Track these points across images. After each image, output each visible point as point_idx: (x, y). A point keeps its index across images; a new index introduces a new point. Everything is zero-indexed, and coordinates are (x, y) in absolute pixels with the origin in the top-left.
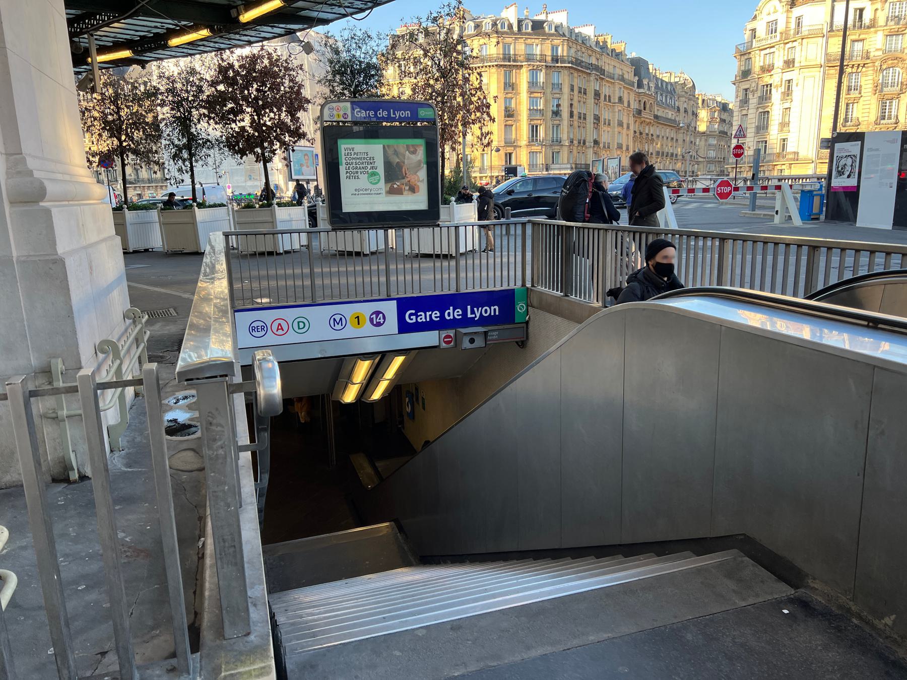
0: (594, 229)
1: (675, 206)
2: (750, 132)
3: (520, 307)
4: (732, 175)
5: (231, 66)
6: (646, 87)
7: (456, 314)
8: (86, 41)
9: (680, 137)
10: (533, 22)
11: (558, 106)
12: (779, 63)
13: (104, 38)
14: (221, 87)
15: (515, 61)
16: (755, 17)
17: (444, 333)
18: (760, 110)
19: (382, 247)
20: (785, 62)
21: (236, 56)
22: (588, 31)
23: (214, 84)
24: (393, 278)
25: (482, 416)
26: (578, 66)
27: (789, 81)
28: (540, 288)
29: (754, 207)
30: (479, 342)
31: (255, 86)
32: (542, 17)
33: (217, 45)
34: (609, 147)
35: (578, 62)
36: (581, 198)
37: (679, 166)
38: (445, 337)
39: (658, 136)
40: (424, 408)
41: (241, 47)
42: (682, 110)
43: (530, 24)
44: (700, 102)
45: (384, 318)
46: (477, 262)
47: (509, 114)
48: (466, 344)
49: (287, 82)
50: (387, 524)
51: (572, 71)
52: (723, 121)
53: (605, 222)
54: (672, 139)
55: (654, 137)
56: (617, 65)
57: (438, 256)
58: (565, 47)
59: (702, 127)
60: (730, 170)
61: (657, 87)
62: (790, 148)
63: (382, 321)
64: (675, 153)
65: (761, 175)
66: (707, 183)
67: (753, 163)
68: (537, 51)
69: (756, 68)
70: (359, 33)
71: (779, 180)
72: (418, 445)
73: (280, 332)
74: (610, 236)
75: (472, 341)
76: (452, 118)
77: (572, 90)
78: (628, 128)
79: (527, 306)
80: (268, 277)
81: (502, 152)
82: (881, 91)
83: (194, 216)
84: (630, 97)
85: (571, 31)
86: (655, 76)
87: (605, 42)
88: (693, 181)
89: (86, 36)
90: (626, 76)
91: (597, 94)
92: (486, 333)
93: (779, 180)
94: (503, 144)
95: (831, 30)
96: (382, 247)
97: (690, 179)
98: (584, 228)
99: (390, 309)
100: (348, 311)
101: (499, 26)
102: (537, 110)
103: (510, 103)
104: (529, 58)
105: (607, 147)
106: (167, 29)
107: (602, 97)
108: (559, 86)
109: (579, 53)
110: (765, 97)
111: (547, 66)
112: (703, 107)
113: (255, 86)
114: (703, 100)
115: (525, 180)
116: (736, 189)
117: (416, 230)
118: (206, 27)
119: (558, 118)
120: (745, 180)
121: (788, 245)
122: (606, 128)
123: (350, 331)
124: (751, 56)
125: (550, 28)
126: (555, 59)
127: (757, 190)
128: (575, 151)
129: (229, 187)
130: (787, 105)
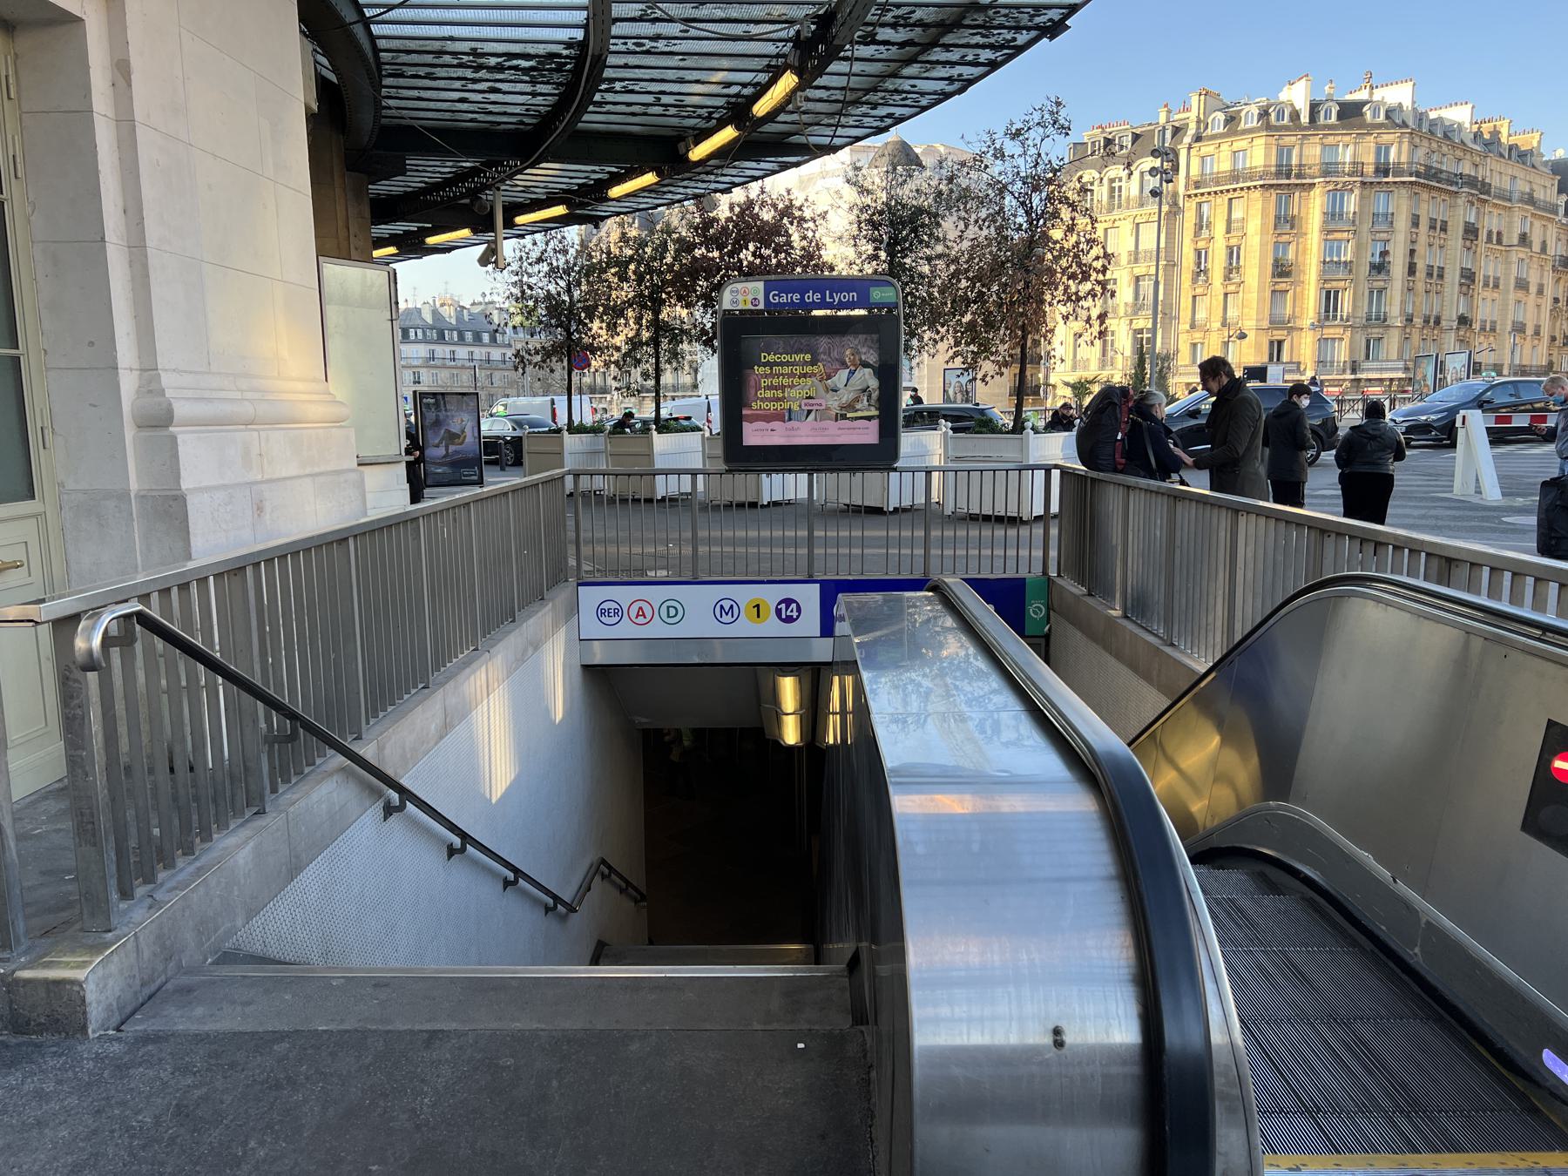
11: (1384, 254)
15: (1299, 176)
19: (920, 500)
22: (1459, 115)
24: (935, 552)
26: (1430, 179)
31: (751, 247)
32: (1362, 95)
34: (1493, 330)
35: (1431, 173)
43: (1335, 110)
45: (799, 609)
47: (1282, 271)
51: (1417, 189)
56: (1520, 174)
57: (987, 518)
58: (1405, 146)
63: (795, 614)
68: (1346, 156)
77: (1416, 224)
78: (1540, 292)
79: (1048, 609)
85: (1420, 117)
87: (1496, 133)
90: (1539, 195)
96: (920, 500)
99: (809, 596)
101: (1273, 116)
102: (1338, 263)
103: (1285, 251)
104: (1328, 170)
107: (1483, 235)
108: (1389, 219)
109: (1435, 157)
111: (1363, 183)
117: (859, 475)
123: (745, 627)
125: (1375, 114)
126: (1383, 170)
128: (1416, 337)
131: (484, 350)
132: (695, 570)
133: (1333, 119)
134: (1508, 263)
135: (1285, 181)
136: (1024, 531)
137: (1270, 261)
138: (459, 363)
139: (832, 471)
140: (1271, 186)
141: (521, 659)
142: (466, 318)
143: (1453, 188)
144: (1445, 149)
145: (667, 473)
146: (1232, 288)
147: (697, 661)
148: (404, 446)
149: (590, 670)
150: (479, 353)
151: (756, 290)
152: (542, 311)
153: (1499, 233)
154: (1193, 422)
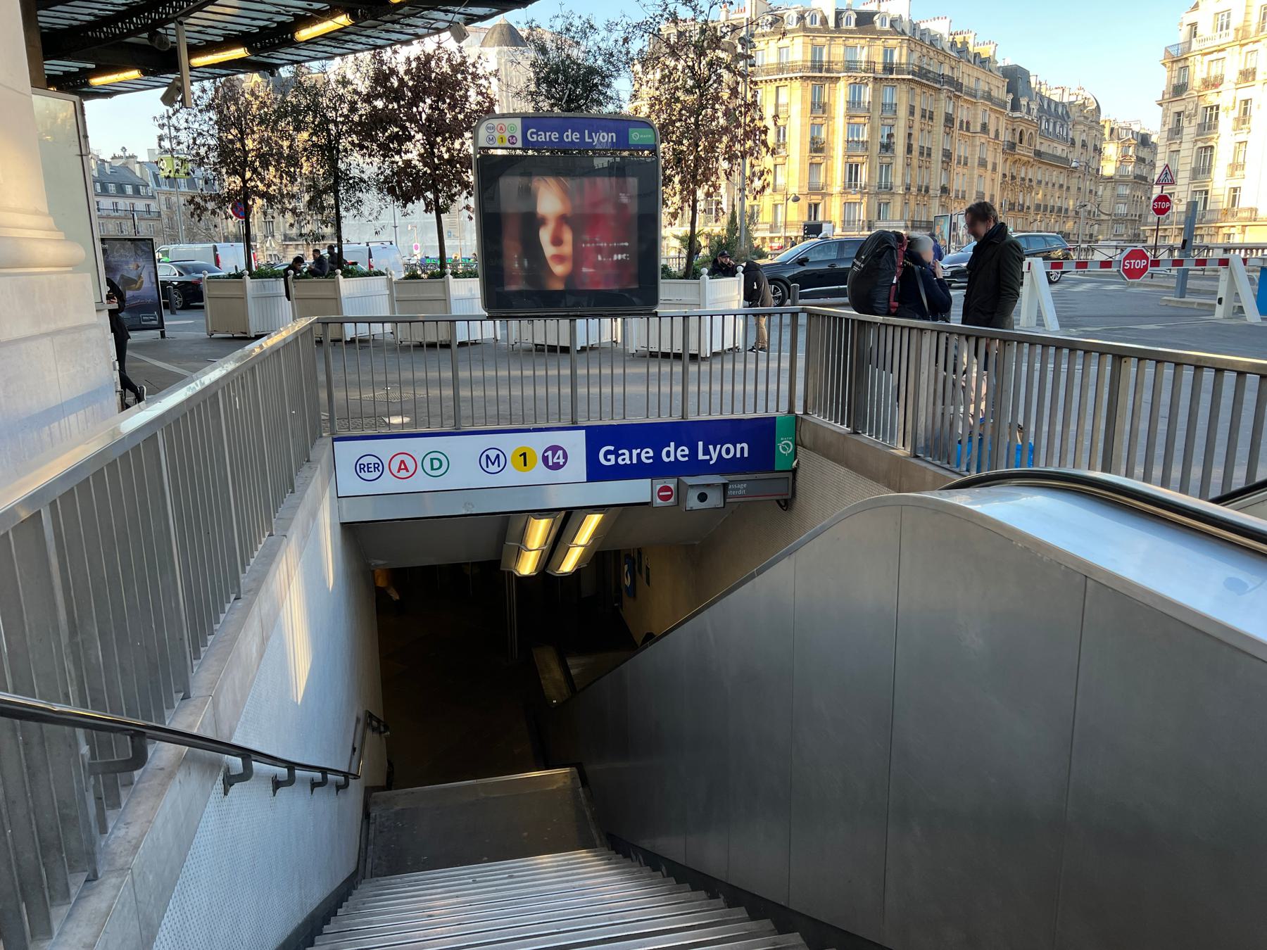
0: (903, 328)
1: (1056, 287)
2: (1183, 178)
3: (784, 446)
4: (1151, 242)
5: (393, 72)
6: (1024, 110)
7: (679, 453)
8: (174, 32)
9: (1074, 183)
10: (858, 13)
11: (890, 136)
12: (1231, 75)
13: (210, 31)
14: (379, 104)
15: (828, 71)
16: (1196, 6)
17: (659, 483)
18: (1200, 144)
20: (1241, 73)
21: (401, 57)
22: (940, 28)
23: (368, 99)
24: (582, 391)
25: (709, 619)
26: (922, 78)
27: (1246, 102)
28: (817, 418)
29: (1183, 291)
30: (715, 500)
31: (428, 101)
32: (872, 7)
33: (371, 41)
35: (922, 73)
36: (886, 276)
37: (1069, 226)
38: (662, 489)
39: (1039, 182)
40: (648, 582)
41: (407, 43)
43: (854, 17)
44: (1107, 131)
46: (739, 367)
47: (817, 147)
48: (693, 502)
49: (472, 93)
50: (567, 770)
52: (1141, 160)
53: (924, 317)
54: (1061, 186)
55: (1034, 183)
56: (982, 77)
57: (666, 356)
58: (905, 51)
59: (1108, 169)
60: (1148, 234)
61: (1041, 109)
62: (1245, 202)
63: (561, 461)
64: (1064, 207)
65: (1197, 242)
66: (1111, 252)
67: (1185, 223)
68: (862, 56)
69: (1196, 82)
70: (577, 22)
71: (1226, 250)
72: (639, 639)
73: (403, 474)
74: (928, 341)
75: (702, 498)
76: (711, 148)
77: (912, 113)
78: (994, 169)
79: (796, 445)
80: (414, 383)
81: (804, 202)
83: (337, 289)
84: (1000, 125)
85: (914, 27)
86: (1039, 94)
87: (965, 43)
88: (1087, 250)
89: (172, 25)
90: (994, 93)
91: (949, 120)
92: (725, 486)
93: (1226, 250)
94: (806, 190)
97: (1084, 246)
98: (887, 325)
99: (575, 443)
100: (510, 444)
102: (858, 142)
103: (819, 132)
104: (850, 66)
106: (294, 15)
107: (957, 124)
108: (893, 108)
109: (925, 60)
110: (1208, 124)
111: (875, 79)
112: (1111, 139)
113: (428, 101)
114: (1112, 130)
115: (827, 244)
116: (1156, 263)
118: (345, 12)
119: (888, 154)
120: (1171, 249)
121: (1241, 374)
122: (960, 170)
123: (512, 475)
124: (1188, 63)
126: (889, 68)
127: (1189, 265)
128: (912, 202)
129: (416, 248)
130: (1241, 138)
131: (128, 201)
132: (457, 417)
133: (853, 26)
134: (974, 146)
135: (818, 74)
136: (705, 367)
137: (808, 139)
138: (104, 213)
139: (593, 316)
140: (808, 78)
141: (305, 536)
142: (108, 171)
143: (937, 86)
144: (932, 54)
145: (355, 321)
146: (780, 160)
147: (464, 512)
148: (105, 293)
149: (345, 526)
150: (123, 203)
151: (513, 128)
152: (213, 157)
153: (968, 123)
154: (802, 269)
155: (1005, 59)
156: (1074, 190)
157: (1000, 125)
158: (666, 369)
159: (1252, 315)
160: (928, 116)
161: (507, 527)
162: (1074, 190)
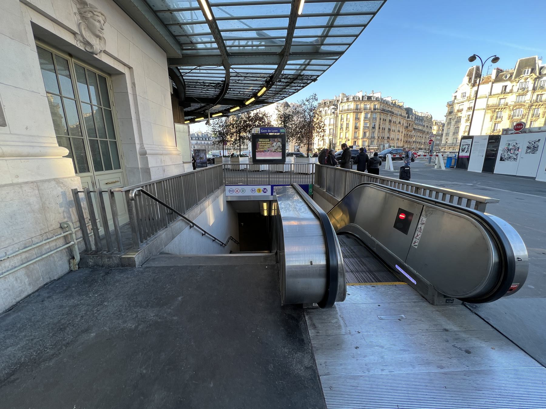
9: (424, 136)
22: (389, 99)
26: (383, 111)
35: (384, 110)
42: (426, 126)
44: (434, 123)
47: (356, 128)
57: (304, 174)
61: (415, 118)
68: (368, 106)
82: (512, 118)
84: (404, 122)
85: (382, 99)
87: (395, 103)
90: (403, 114)
95: (491, 95)
100: (257, 188)
105: (393, 139)
110: (458, 121)
122: (393, 133)
123: (257, 194)
126: (375, 109)
135: (357, 111)
136: (309, 176)
150: (206, 142)
155: (406, 106)
156: (424, 138)
157: (404, 122)
158: (304, 176)
159: (443, 168)
160: (385, 120)
161: (258, 203)
162: (424, 138)
